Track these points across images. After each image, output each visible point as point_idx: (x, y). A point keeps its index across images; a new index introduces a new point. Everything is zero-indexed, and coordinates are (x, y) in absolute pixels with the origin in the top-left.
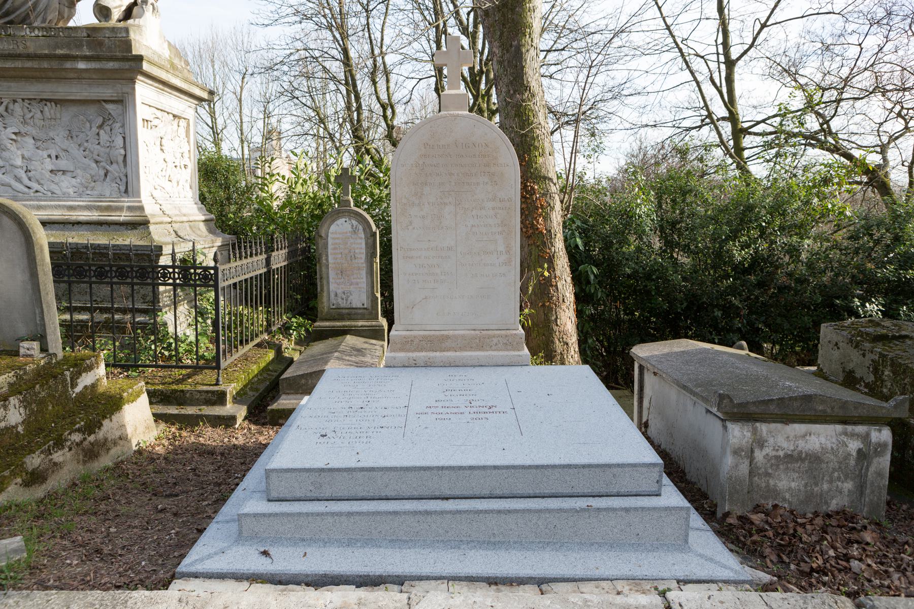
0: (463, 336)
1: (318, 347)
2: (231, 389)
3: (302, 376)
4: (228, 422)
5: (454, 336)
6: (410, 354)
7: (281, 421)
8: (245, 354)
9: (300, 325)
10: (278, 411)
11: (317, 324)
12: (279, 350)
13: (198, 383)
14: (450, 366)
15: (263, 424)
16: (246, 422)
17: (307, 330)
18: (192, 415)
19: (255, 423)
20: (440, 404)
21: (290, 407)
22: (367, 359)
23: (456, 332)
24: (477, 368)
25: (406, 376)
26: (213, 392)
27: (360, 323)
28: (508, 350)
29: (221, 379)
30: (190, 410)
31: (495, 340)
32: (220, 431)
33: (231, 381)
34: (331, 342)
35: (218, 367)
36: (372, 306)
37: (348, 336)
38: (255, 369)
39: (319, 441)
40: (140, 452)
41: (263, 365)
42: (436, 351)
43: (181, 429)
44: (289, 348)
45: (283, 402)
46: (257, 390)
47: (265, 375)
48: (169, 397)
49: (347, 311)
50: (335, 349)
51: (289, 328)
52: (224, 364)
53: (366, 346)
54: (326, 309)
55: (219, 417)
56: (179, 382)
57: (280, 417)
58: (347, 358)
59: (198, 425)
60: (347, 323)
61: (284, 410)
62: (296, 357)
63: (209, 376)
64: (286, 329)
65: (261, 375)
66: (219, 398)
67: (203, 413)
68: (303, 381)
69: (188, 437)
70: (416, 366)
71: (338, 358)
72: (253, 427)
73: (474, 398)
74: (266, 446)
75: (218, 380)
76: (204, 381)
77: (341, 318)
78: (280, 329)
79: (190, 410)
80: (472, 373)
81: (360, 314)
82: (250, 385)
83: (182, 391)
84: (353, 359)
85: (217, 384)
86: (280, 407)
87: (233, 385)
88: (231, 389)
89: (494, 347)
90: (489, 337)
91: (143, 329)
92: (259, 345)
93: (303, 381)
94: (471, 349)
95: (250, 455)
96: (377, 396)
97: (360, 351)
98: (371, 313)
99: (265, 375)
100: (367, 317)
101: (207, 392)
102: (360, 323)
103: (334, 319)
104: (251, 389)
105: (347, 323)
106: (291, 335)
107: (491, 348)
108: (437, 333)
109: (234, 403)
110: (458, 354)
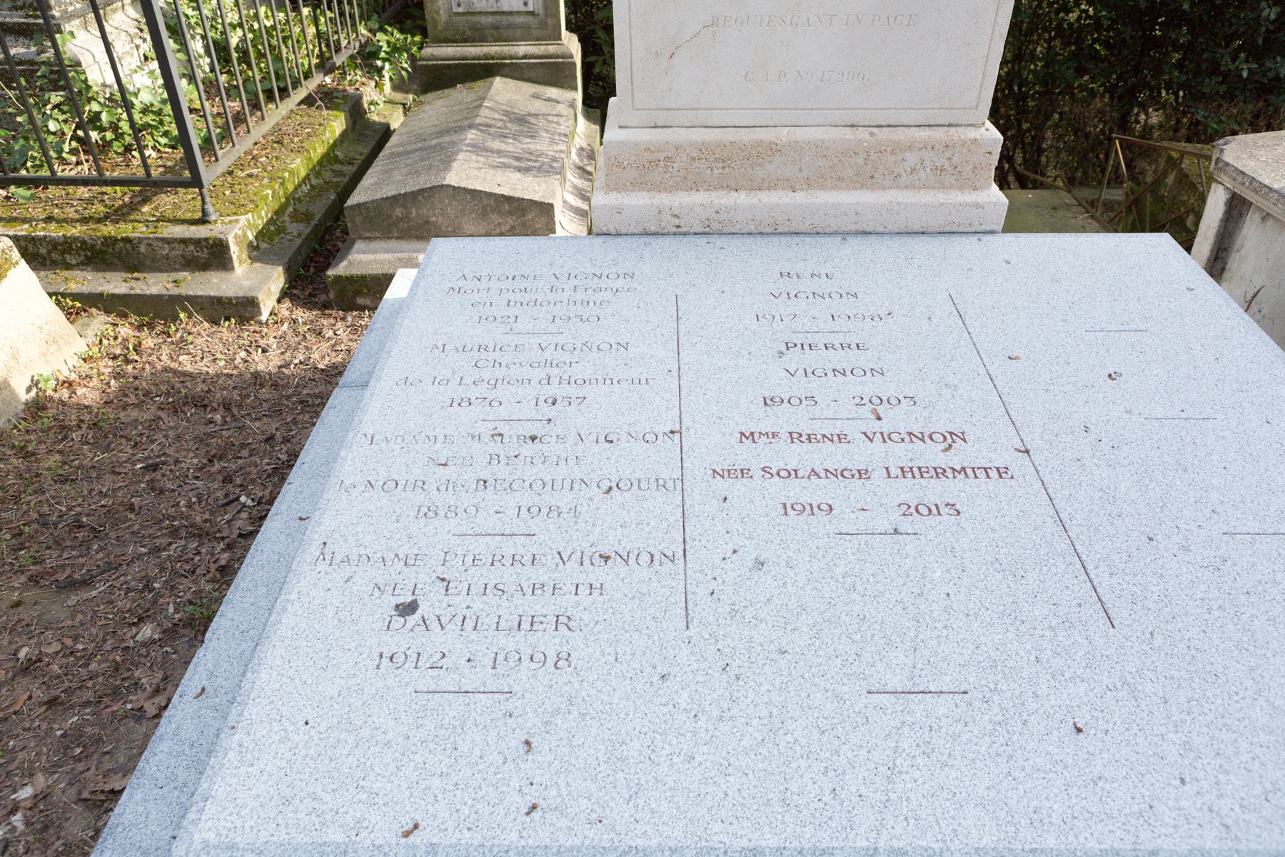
0: (819, 146)
1: (439, 106)
2: (237, 231)
3: (395, 200)
4: (243, 310)
5: (793, 145)
6: (663, 199)
7: (360, 301)
8: (277, 128)
9: (395, 49)
10: (350, 279)
11: (428, 51)
12: (356, 111)
13: (162, 219)
14: (776, 233)
15: (325, 306)
16: (287, 303)
17: (412, 59)
18: (159, 298)
19: (308, 304)
20: (783, 419)
21: (377, 270)
22: (541, 145)
23: (801, 134)
24: (854, 242)
25: (658, 266)
26: (197, 242)
27: (522, 49)
28: (943, 187)
29: (210, 208)
30: (155, 284)
31: (912, 158)
32: (226, 330)
33: (238, 208)
34: (460, 94)
35: (196, 182)
36: (546, 8)
37: (498, 82)
38: (299, 166)
39: (392, 643)
40: (37, 407)
41: (319, 150)
42: (733, 191)
43: (140, 328)
44: (380, 99)
45: (361, 259)
46: (307, 217)
47: (327, 175)
48: (102, 252)
49: (490, 19)
50: (466, 121)
51: (374, 55)
52: (209, 173)
53: (538, 106)
54: (443, 16)
55: (218, 301)
56: (119, 214)
57: (359, 293)
58: (497, 145)
59: (175, 318)
60: (494, 49)
61: (363, 278)
62: (396, 120)
63: (185, 201)
64: (367, 58)
65: (318, 175)
66: (214, 256)
67: (184, 290)
68: (398, 212)
69: (158, 352)
70: (679, 233)
71: (477, 148)
72: (301, 315)
73: (887, 387)
74: (333, 374)
75: (204, 211)
76: (166, 218)
77: (477, 35)
78: (352, 57)
79: (155, 284)
80: (847, 260)
81: (522, 26)
82: (292, 207)
83: (127, 240)
84: (510, 146)
85: (203, 221)
86: (356, 271)
87: (243, 219)
88: (237, 231)
89: (904, 179)
90: (897, 149)
91: (29, 76)
92: (308, 101)
93: (398, 212)
94: (839, 182)
95: (298, 403)
96: (578, 372)
97: (523, 122)
98: (543, 25)
99: (327, 175)
100: (535, 33)
101: (184, 241)
102: (522, 49)
103: (465, 40)
104: (296, 217)
105: (494, 49)
106: (380, 71)
107: (896, 181)
108: (744, 136)
109: (253, 259)
110: (800, 198)
